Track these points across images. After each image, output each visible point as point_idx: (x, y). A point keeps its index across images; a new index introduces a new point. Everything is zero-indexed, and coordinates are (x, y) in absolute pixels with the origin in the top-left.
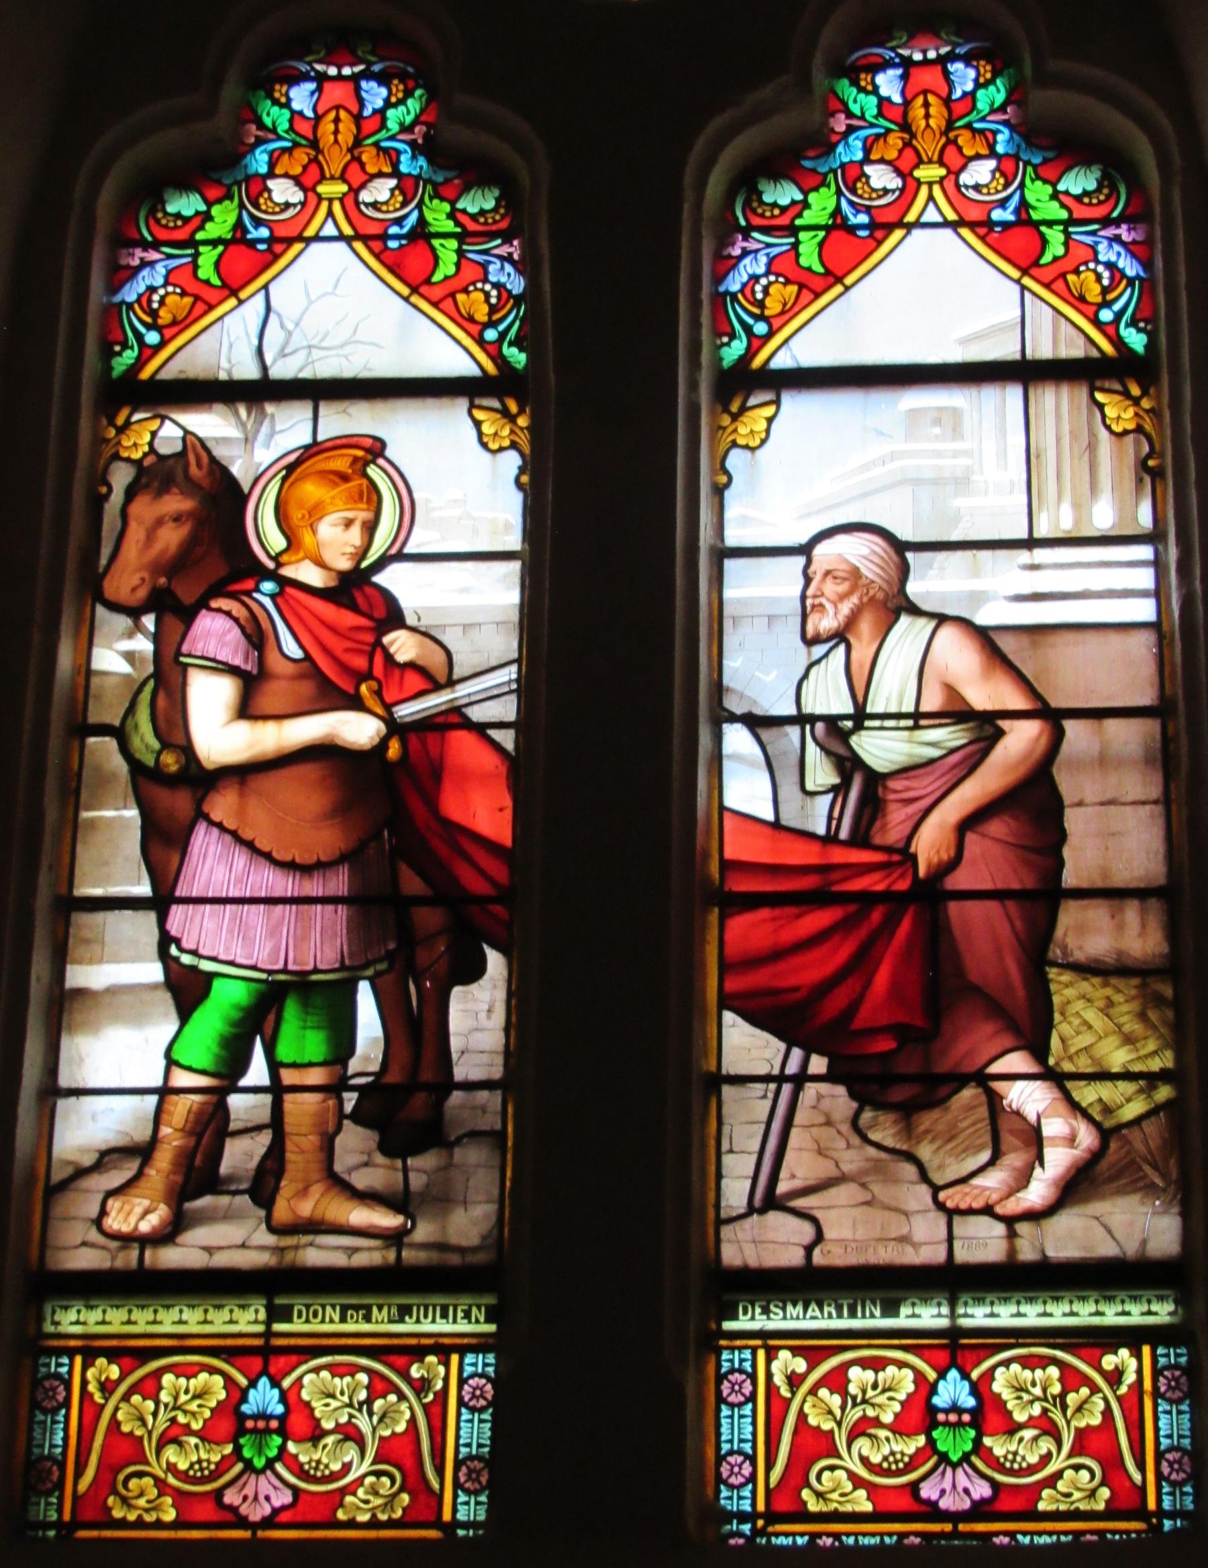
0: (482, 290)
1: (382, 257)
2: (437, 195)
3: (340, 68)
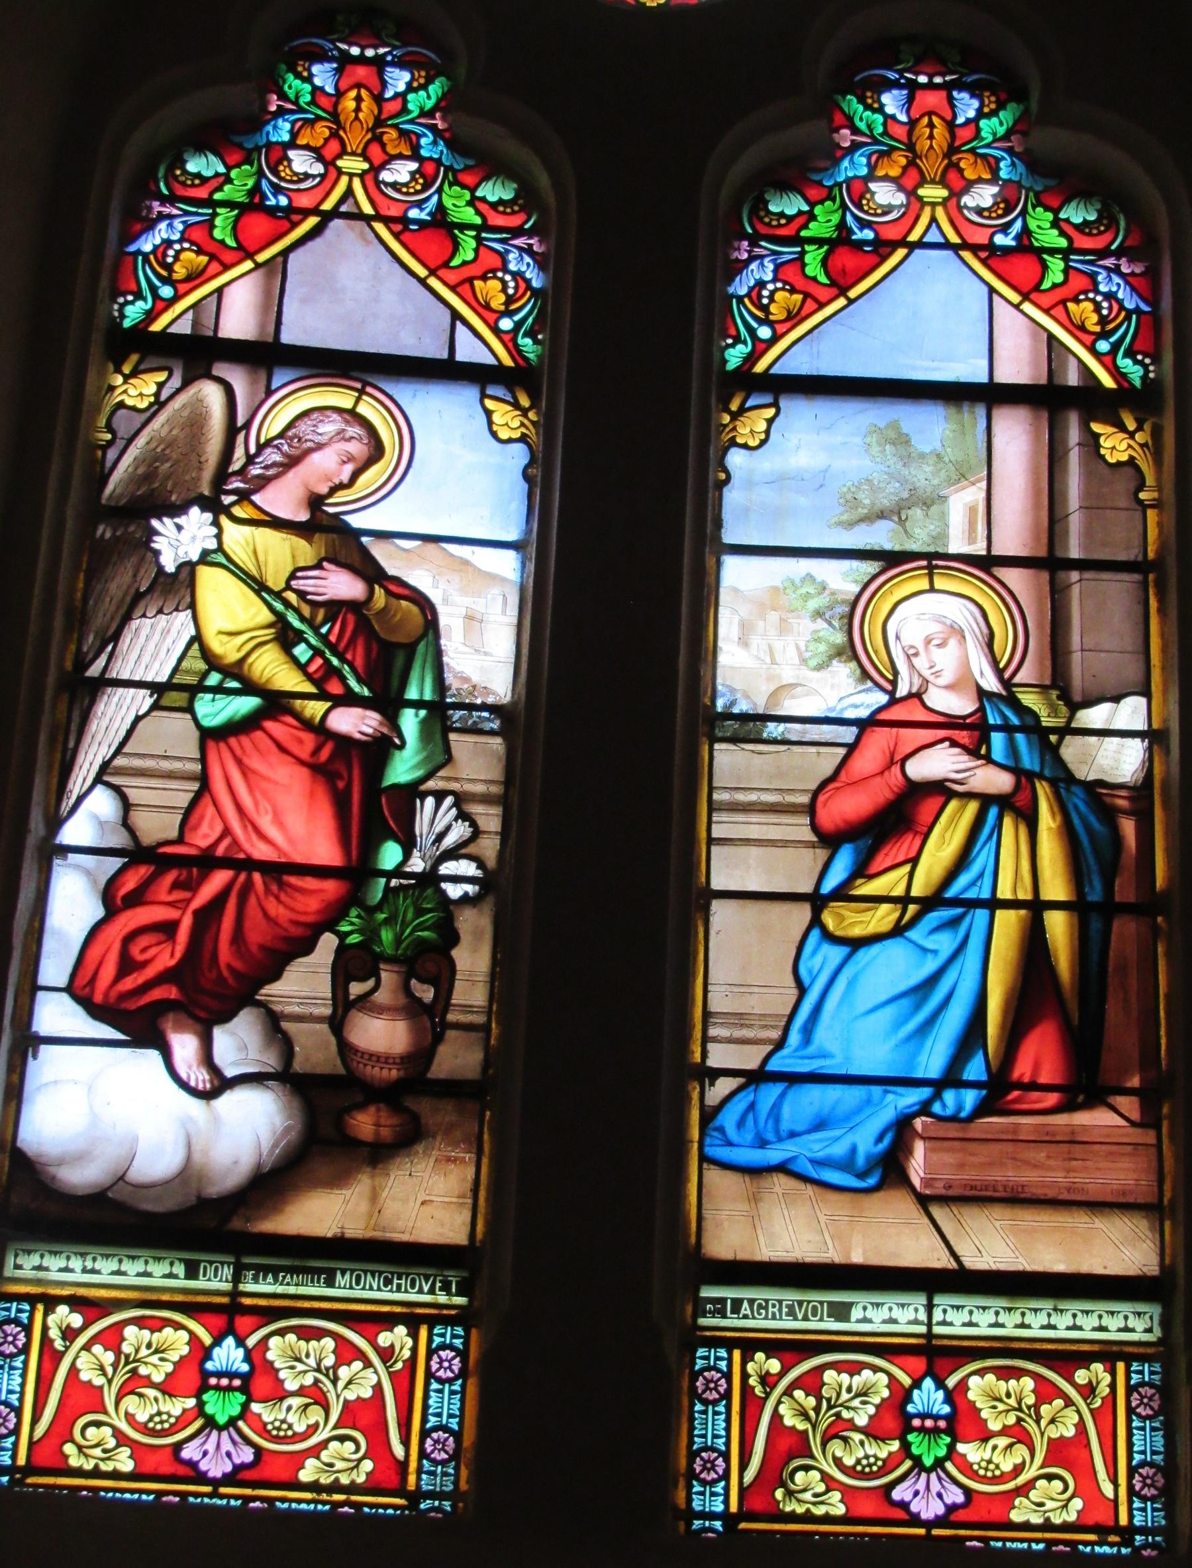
0: (1093, 301)
1: (402, 237)
2: (1039, 203)
3: (363, 48)
